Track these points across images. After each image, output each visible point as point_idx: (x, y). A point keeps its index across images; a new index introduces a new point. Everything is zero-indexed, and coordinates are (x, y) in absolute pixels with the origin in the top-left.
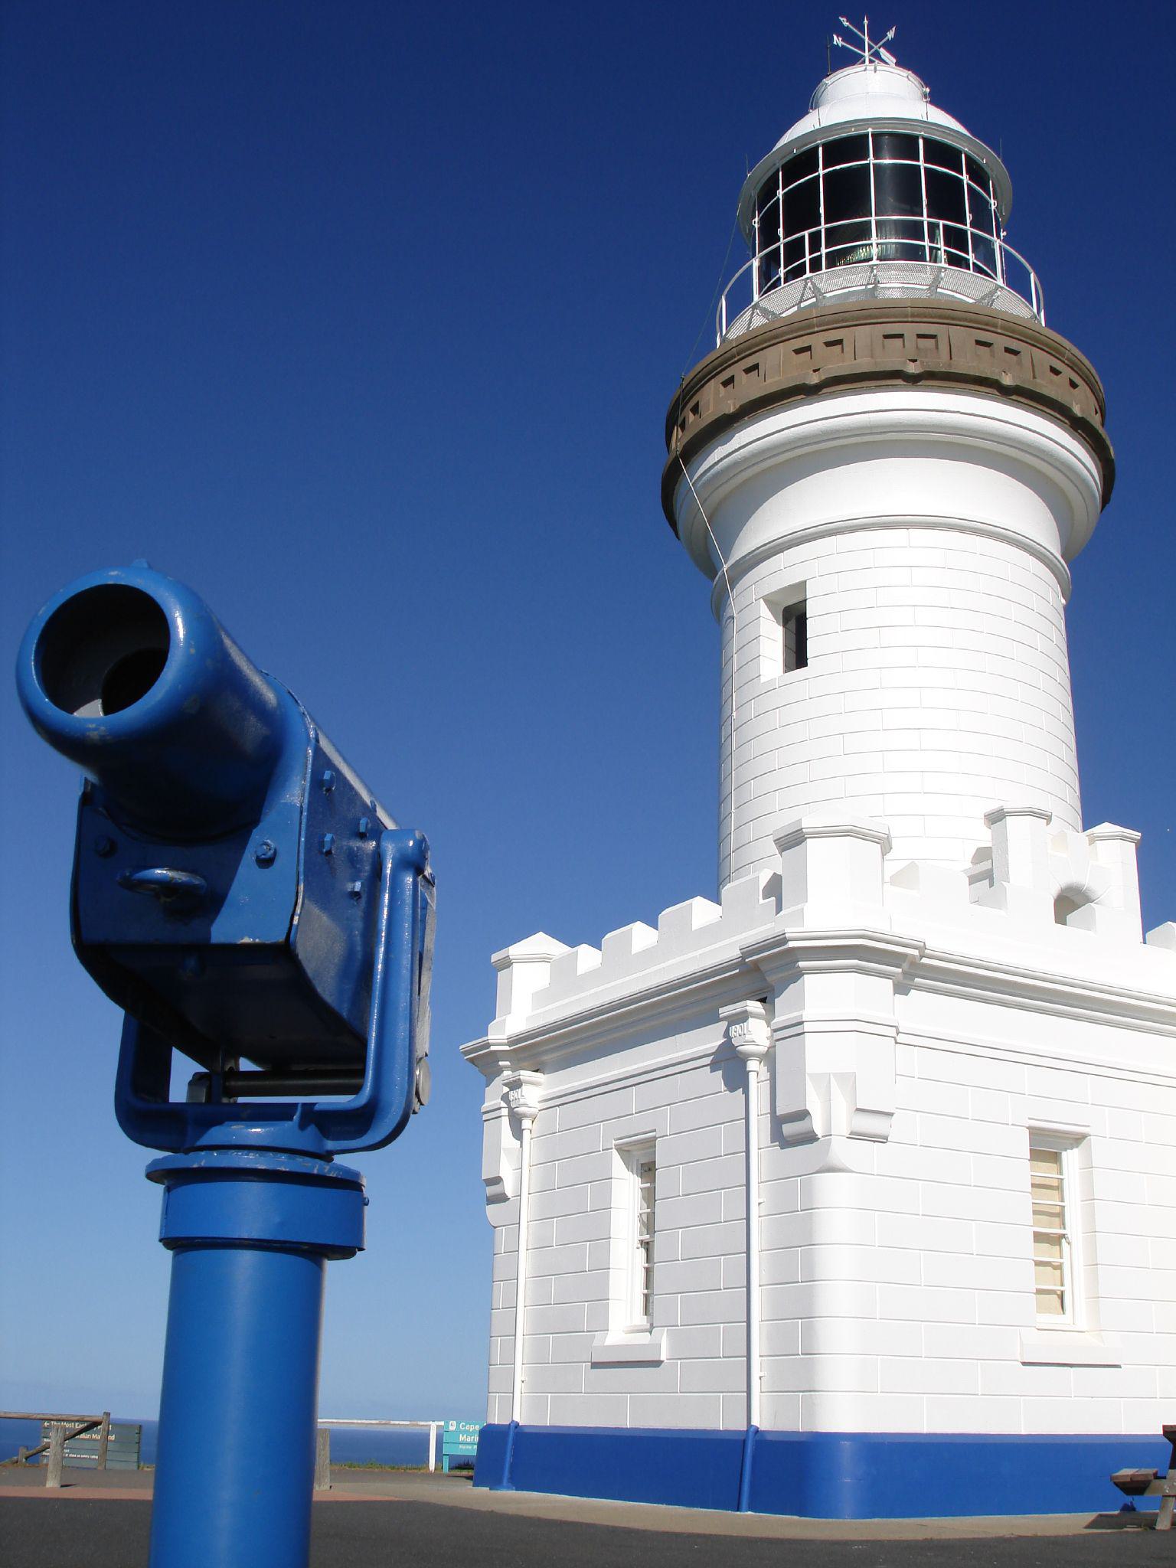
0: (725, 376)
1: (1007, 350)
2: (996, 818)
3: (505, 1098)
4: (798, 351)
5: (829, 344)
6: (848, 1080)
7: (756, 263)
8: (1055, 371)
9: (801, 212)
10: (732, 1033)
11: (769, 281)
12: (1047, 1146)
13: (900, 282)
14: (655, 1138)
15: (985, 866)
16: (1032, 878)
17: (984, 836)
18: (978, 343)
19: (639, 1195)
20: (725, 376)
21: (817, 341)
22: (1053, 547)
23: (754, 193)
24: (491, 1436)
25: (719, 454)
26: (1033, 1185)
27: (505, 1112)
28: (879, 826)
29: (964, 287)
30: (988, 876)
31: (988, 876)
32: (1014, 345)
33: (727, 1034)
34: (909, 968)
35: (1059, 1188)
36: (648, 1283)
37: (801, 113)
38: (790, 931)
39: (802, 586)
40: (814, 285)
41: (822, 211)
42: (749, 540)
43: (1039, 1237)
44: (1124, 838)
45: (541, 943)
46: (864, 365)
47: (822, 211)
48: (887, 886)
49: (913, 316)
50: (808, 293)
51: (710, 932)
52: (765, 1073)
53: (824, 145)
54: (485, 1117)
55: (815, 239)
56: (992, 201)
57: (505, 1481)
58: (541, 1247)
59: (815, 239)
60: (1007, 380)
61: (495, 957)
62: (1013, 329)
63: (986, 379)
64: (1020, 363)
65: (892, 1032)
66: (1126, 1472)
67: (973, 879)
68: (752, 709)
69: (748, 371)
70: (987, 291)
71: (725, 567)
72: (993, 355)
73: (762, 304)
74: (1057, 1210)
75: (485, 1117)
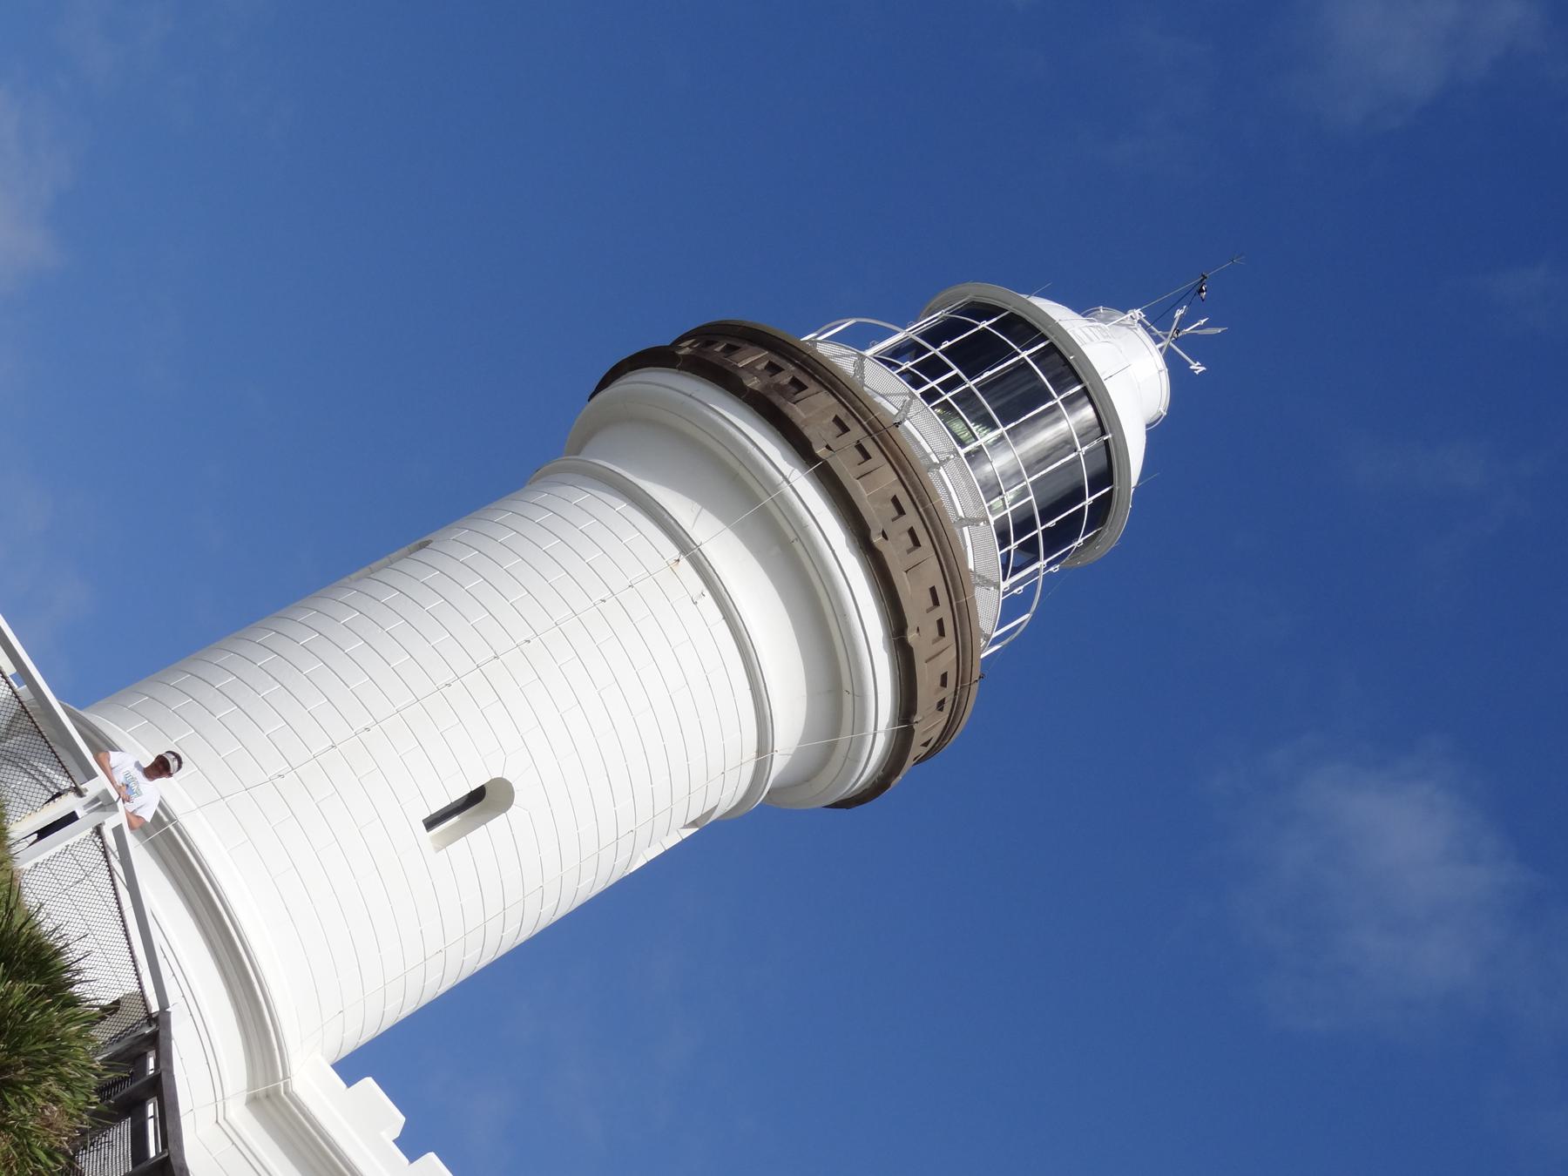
1: (940, 622)
9: (975, 354)
11: (890, 359)
21: (912, 519)
37: (1082, 307)
40: (910, 404)
41: (986, 375)
47: (986, 375)
55: (956, 381)
59: (956, 381)
60: (911, 637)
62: (963, 614)
63: (884, 561)
68: (268, 659)
70: (988, 576)
73: (866, 362)
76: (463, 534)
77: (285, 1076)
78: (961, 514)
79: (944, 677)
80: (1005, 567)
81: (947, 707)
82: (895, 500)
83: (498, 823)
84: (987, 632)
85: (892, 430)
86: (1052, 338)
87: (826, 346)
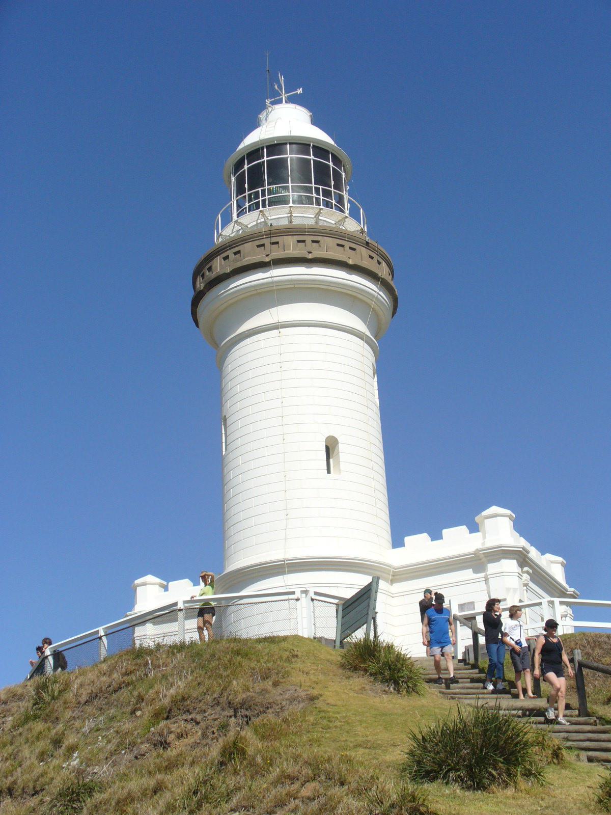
1: (351, 248)
4: (258, 246)
8: (371, 257)
9: (256, 178)
29: (329, 218)
32: (353, 246)
37: (255, 124)
55: (263, 192)
56: (343, 174)
59: (263, 192)
60: (351, 262)
62: (351, 238)
68: (240, 498)
72: (356, 254)
76: (228, 404)
77: (390, 567)
78: (313, 216)
81: (381, 260)
82: (299, 241)
83: (341, 447)
84: (359, 228)
85: (273, 228)
86: (265, 145)
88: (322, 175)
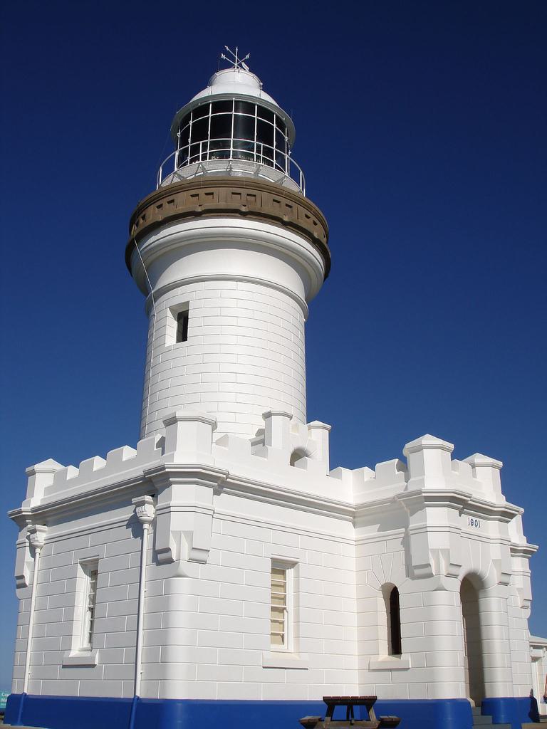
0: (159, 203)
1: (287, 205)
2: (267, 416)
3: (28, 537)
4: (192, 196)
5: (207, 194)
6: (190, 535)
7: (177, 153)
9: (200, 132)
10: (137, 511)
12: (280, 567)
13: (242, 169)
14: (98, 559)
15: (262, 437)
16: (281, 445)
17: (261, 424)
18: (274, 200)
19: (89, 585)
20: (159, 203)
21: (201, 192)
22: (302, 295)
23: (179, 121)
24: (13, 700)
25: (153, 239)
26: (272, 585)
27: (28, 544)
28: (210, 417)
29: (270, 175)
30: (263, 442)
31: (263, 442)
32: (290, 203)
33: (135, 511)
34: (221, 483)
35: (284, 586)
36: (92, 628)
38: (167, 464)
39: (187, 303)
42: (165, 280)
43: (273, 609)
44: (323, 428)
45: (51, 464)
46: (222, 205)
48: (214, 445)
49: (246, 185)
50: (200, 170)
51: (131, 462)
52: (151, 531)
53: (213, 103)
54: (18, 546)
56: (286, 137)
57: (19, 721)
58: (41, 609)
59: (205, 146)
60: (286, 219)
61: (27, 470)
62: (290, 195)
64: (292, 211)
65: (211, 513)
66: (307, 718)
67: (254, 444)
68: (160, 359)
69: (169, 202)
71: (153, 292)
72: (280, 207)
74: (283, 597)
75: (18, 546)
79: (307, 216)
80: (282, 171)
87: (165, 183)
88: (265, 134)
